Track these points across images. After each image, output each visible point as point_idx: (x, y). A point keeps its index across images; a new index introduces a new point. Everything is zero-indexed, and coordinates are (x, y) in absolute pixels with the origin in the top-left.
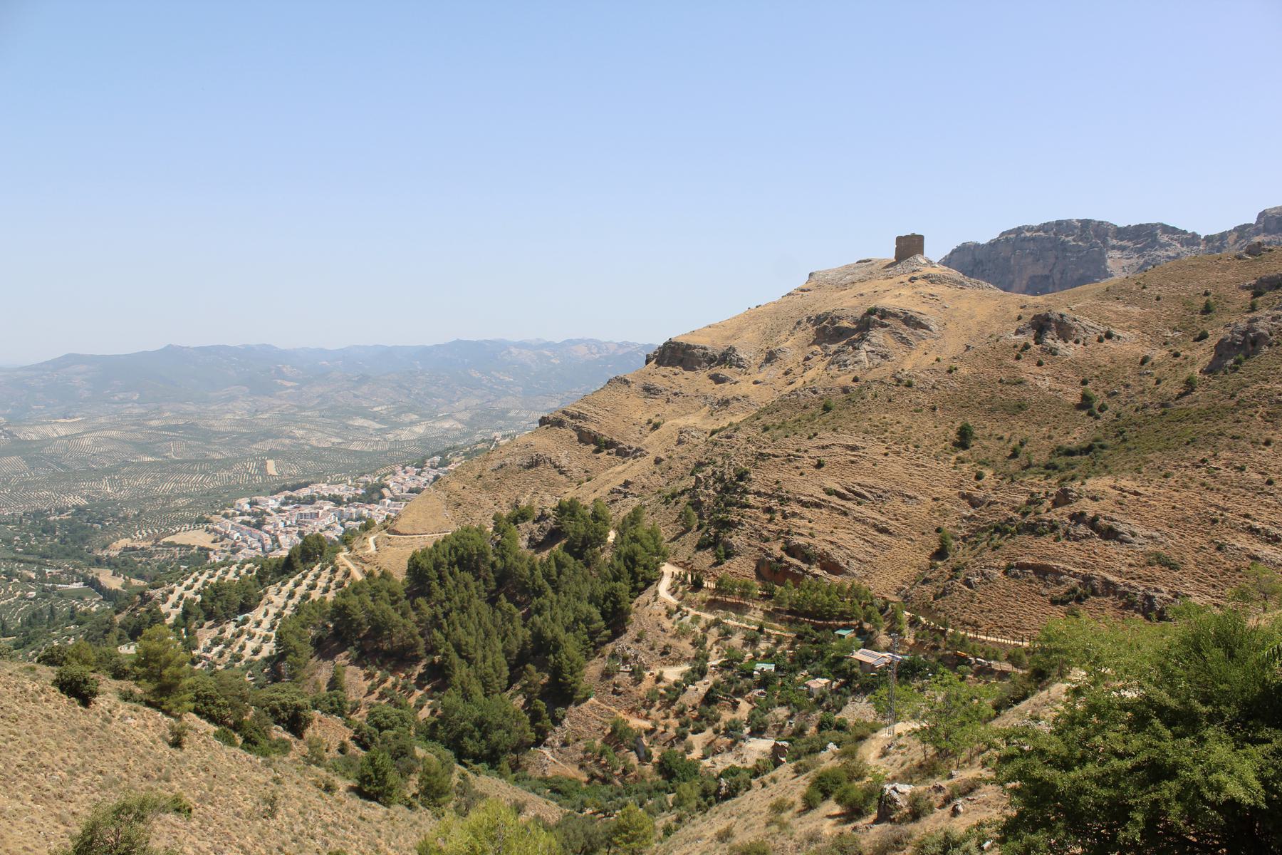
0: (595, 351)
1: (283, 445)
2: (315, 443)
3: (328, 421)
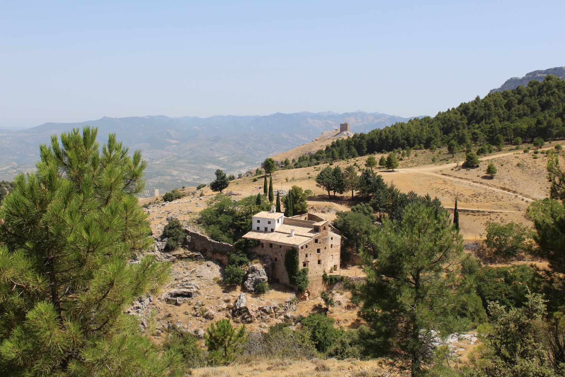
0: (360, 121)
1: (166, 180)
2: (184, 179)
3: (193, 166)
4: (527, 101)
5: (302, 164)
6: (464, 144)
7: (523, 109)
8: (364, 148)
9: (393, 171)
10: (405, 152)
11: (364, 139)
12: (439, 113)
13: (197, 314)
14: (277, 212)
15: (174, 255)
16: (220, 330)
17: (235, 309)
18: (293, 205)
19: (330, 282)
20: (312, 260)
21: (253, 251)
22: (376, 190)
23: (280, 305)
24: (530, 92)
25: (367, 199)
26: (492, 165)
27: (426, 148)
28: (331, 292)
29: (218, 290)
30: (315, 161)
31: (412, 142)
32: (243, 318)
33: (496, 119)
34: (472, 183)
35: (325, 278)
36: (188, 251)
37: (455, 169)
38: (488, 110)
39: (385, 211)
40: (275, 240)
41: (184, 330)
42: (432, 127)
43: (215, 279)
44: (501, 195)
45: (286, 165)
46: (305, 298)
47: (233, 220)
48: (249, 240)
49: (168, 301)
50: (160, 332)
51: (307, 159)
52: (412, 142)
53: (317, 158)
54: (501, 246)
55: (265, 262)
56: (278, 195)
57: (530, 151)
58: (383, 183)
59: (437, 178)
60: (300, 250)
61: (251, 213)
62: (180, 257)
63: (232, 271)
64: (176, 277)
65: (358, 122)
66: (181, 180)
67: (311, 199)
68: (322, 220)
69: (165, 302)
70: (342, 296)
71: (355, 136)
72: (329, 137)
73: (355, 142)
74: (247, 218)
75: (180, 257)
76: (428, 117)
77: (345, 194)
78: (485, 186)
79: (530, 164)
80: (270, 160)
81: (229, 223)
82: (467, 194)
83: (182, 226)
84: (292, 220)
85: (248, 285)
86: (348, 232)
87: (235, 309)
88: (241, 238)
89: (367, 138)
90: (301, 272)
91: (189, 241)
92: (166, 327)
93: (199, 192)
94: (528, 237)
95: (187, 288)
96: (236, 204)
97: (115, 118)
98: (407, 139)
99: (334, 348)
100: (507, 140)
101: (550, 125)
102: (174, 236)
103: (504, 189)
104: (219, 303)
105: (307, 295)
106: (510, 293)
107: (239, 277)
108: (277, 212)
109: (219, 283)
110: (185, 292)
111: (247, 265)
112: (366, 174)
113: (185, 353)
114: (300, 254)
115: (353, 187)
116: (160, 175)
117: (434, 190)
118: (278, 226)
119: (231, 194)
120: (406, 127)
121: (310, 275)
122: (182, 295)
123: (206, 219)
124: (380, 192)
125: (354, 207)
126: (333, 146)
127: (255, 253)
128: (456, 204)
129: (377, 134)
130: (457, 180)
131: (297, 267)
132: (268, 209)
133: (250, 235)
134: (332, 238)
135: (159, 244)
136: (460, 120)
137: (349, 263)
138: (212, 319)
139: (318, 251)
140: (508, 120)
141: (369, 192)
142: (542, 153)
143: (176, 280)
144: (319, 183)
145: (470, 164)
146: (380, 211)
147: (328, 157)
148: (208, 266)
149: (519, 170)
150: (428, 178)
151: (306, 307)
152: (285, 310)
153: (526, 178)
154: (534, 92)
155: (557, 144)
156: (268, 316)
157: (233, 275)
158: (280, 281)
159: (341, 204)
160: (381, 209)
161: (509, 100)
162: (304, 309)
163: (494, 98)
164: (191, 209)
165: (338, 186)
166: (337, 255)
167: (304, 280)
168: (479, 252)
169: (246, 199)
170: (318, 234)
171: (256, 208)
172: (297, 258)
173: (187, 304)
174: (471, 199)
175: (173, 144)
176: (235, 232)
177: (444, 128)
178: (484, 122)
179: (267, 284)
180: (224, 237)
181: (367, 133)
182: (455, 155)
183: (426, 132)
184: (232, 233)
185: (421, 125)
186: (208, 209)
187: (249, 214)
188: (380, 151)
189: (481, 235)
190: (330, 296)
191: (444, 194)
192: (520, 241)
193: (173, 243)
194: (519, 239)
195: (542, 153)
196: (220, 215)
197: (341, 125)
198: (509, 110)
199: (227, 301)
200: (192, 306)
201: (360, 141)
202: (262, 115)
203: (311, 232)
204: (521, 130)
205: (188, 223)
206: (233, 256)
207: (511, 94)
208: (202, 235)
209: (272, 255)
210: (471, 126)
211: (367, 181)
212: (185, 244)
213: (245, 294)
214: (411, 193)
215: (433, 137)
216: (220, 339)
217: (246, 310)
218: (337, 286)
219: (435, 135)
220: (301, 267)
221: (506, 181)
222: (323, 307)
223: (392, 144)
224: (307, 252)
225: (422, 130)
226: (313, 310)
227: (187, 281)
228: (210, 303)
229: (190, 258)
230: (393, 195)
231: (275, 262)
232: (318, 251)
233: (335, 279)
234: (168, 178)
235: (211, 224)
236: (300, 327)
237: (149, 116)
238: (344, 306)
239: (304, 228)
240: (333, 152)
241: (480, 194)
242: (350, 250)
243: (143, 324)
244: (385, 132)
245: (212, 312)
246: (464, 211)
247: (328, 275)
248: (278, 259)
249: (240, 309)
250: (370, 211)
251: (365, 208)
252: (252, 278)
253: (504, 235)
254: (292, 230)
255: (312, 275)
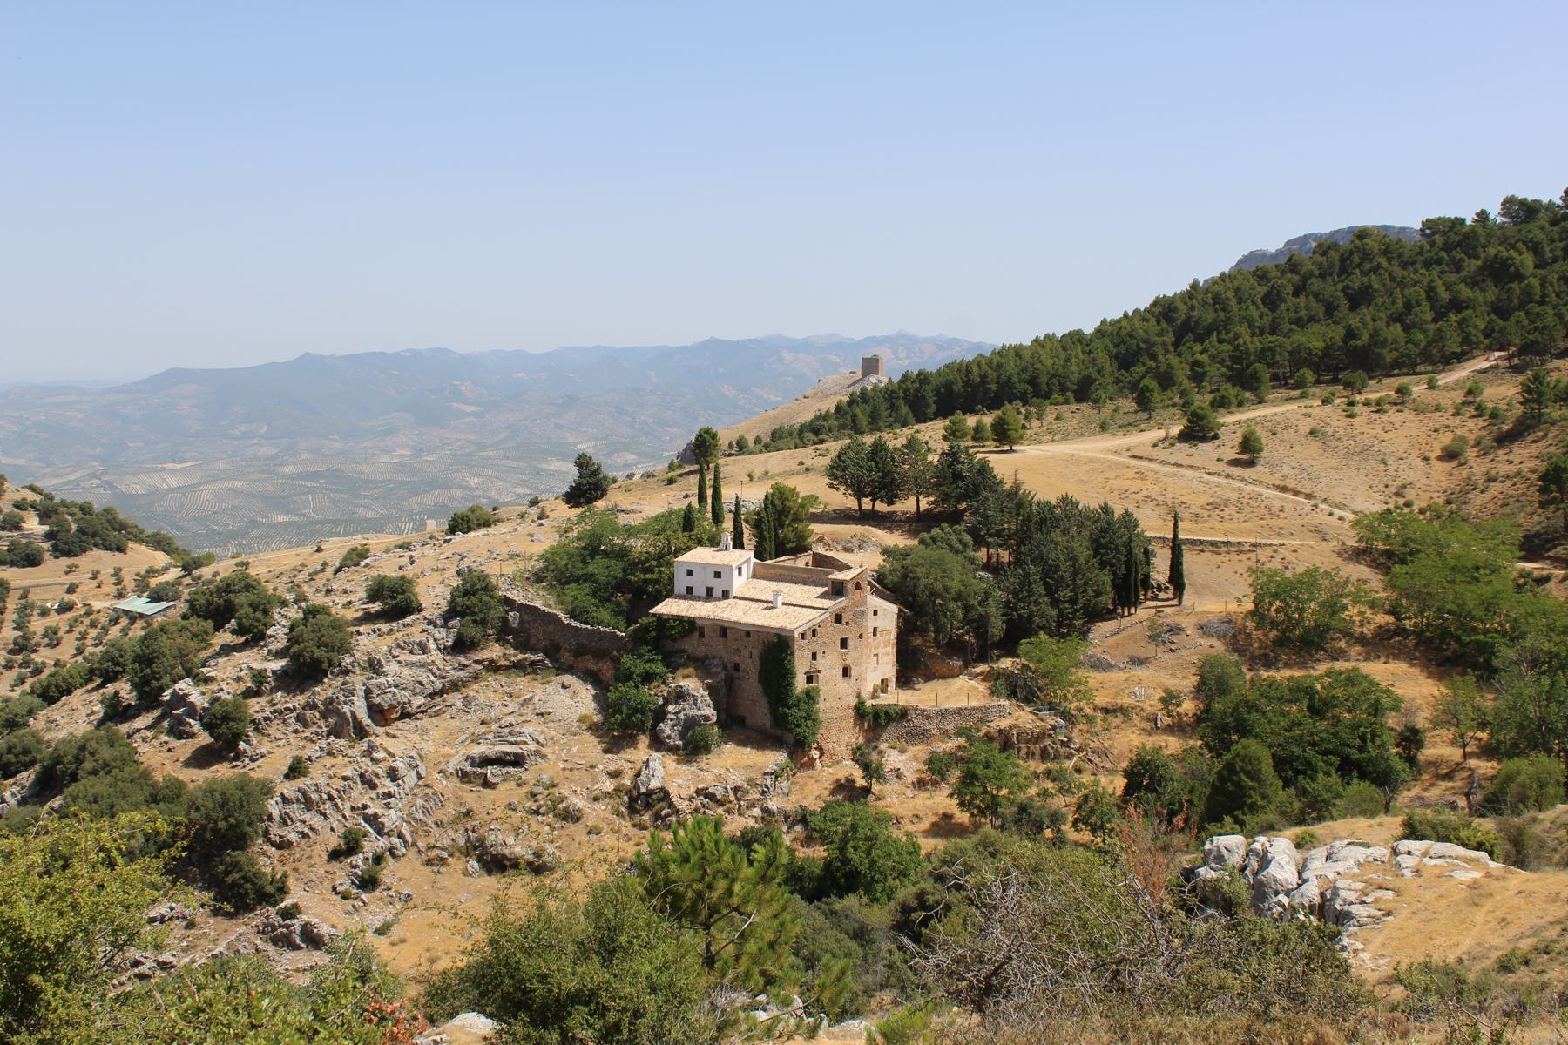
0: (903, 355)
1: (453, 498)
2: (494, 495)
3: (515, 464)
4: (1314, 289)
5: (780, 444)
7: (1307, 307)
8: (928, 406)
9: (1012, 451)
12: (1104, 322)
13: (539, 807)
15: (477, 662)
16: (686, 859)
17: (635, 793)
20: (829, 666)
21: (677, 646)
22: (977, 493)
23: (750, 782)
24: (1320, 266)
25: (955, 518)
26: (1253, 433)
27: (1079, 400)
29: (592, 746)
30: (810, 436)
31: (1044, 387)
32: (657, 816)
33: (1243, 329)
34: (1207, 477)
35: (860, 711)
36: (513, 651)
38: (1224, 310)
39: (1000, 546)
40: (734, 619)
41: (506, 851)
42: (1090, 352)
43: (582, 720)
44: (1277, 504)
45: (741, 447)
46: (811, 764)
48: (667, 620)
49: (464, 776)
50: (445, 855)
52: (1044, 387)
53: (816, 431)
54: (1290, 624)
55: (709, 675)
56: (737, 513)
57: (1337, 401)
59: (1119, 466)
60: (799, 642)
61: (669, 553)
62: (493, 667)
63: (624, 698)
64: (484, 716)
69: (456, 780)
70: (903, 757)
71: (905, 378)
74: (659, 566)
75: (493, 667)
76: (1079, 332)
77: (898, 507)
78: (1237, 484)
79: (1341, 431)
80: (708, 431)
82: (1197, 502)
83: (496, 588)
84: (773, 567)
85: (668, 731)
86: (914, 596)
87: (635, 793)
88: (647, 615)
89: (935, 382)
90: (802, 696)
91: (515, 625)
92: (462, 842)
93: (535, 511)
94: (1355, 603)
96: (630, 531)
97: (332, 356)
98: (1033, 382)
99: (912, 890)
100: (1275, 378)
101: (1377, 340)
103: (1284, 489)
104: (595, 780)
105: (815, 754)
106: (1323, 740)
109: (594, 728)
110: (507, 753)
111: (664, 682)
112: (952, 456)
113: (612, 1017)
114: (797, 653)
115: (920, 488)
118: (739, 584)
119: (616, 510)
120: (1027, 355)
121: (823, 706)
122: (500, 761)
123: (556, 569)
124: (987, 498)
125: (925, 535)
126: (851, 403)
127: (684, 651)
128: (1176, 526)
130: (1168, 469)
131: (791, 684)
132: (714, 542)
133: (669, 607)
134: (875, 613)
135: (440, 633)
136: (1158, 334)
137: (918, 675)
138: (578, 819)
139: (844, 643)
140: (1273, 333)
141: (959, 500)
142: (1367, 404)
143: (483, 722)
144: (836, 478)
145: (1198, 431)
146: (988, 546)
147: (842, 427)
148: (564, 687)
149: (1313, 446)
151: (816, 786)
153: (1333, 463)
154: (1331, 266)
155: (1396, 385)
156: (720, 810)
157: (630, 708)
158: (749, 721)
159: (890, 529)
161: (1273, 287)
162: (811, 790)
163: (1236, 283)
164: (517, 547)
165: (882, 486)
167: (808, 717)
168: (1237, 642)
169: (656, 519)
170: (842, 602)
171: (681, 538)
172: (791, 663)
174: (1206, 513)
175: (468, 415)
176: (630, 602)
178: (1214, 337)
179: (716, 729)
185: (1064, 348)
186: (561, 546)
187: (665, 557)
188: (969, 410)
189: (1239, 600)
190: (874, 757)
192: (1333, 613)
193: (473, 632)
194: (1334, 608)
195: (1367, 404)
198: (1272, 310)
200: (525, 789)
201: (918, 390)
203: (823, 596)
204: (1310, 354)
205: (512, 581)
206: (628, 661)
207: (1274, 273)
209: (725, 656)
210: (1183, 348)
213: (659, 755)
214: (1065, 500)
215: (1095, 375)
216: (690, 894)
217: (664, 795)
219: (1099, 372)
220: (800, 684)
221: (1286, 470)
223: (996, 393)
225: (1067, 360)
226: (832, 793)
227: (511, 725)
228: (572, 781)
229: (519, 666)
230: (1020, 505)
231: (735, 674)
232: (844, 643)
233: (887, 713)
234: (458, 493)
236: (802, 836)
237: (409, 351)
240: (854, 416)
241: (1226, 503)
242: (919, 641)
243: (400, 836)
244: (979, 365)
245: (578, 802)
246: (1193, 542)
247: (869, 703)
248: (742, 667)
249: (650, 793)
250: (965, 545)
251: (954, 538)
253: (1296, 598)
254: (776, 593)
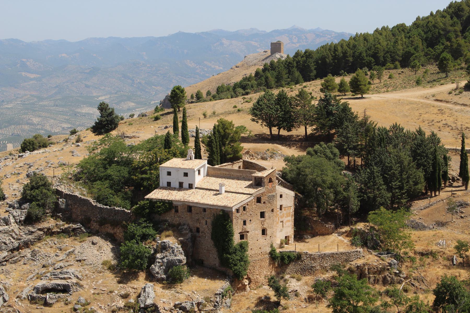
0: (295, 41)
2: (48, 128)
3: (61, 109)
6: (462, 58)
8: (311, 71)
9: (362, 98)
10: (375, 72)
11: (311, 58)
12: (418, 19)
14: (196, 158)
15: (40, 230)
18: (220, 148)
19: (282, 261)
20: (254, 228)
21: (162, 218)
22: (342, 123)
23: (207, 299)
25: (328, 138)
27: (403, 66)
28: (283, 277)
29: (110, 280)
30: (240, 90)
31: (382, 59)
35: (273, 256)
36: (62, 223)
37: (454, 93)
39: (356, 155)
40: (196, 201)
42: (409, 37)
43: (104, 263)
45: (198, 98)
47: (129, 173)
48: (156, 202)
49: (32, 300)
51: (228, 90)
52: (382, 59)
53: (244, 88)
55: (181, 235)
58: (352, 114)
59: (428, 106)
60: (235, 215)
62: (49, 232)
63: (130, 250)
64: (44, 263)
65: (293, 43)
66: (45, 130)
67: (245, 140)
68: (264, 169)
69: (27, 302)
70: (299, 283)
72: (255, 62)
73: (297, 63)
74: (150, 170)
75: (49, 232)
77: (294, 132)
80: (178, 88)
81: (124, 177)
83: (51, 184)
84: (219, 169)
86: (304, 186)
88: (144, 199)
89: (315, 56)
90: (238, 247)
91: (63, 207)
95: (61, 279)
96: (132, 149)
98: (375, 56)
102: (39, 200)
104: (113, 300)
105: (246, 282)
107: (141, 259)
108: (196, 158)
109: (112, 269)
110: (59, 285)
111: (154, 240)
112: (326, 101)
114: (234, 221)
115: (307, 121)
116: (14, 124)
117: (427, 122)
118: (199, 180)
119: (124, 136)
120: (371, 40)
124: (347, 127)
125: (310, 149)
126: (265, 70)
127: (166, 221)
129: (330, 50)
130: (458, 107)
131: (231, 240)
132: (183, 155)
133: (157, 195)
134: (281, 196)
135: (17, 213)
139: (262, 215)
141: (331, 128)
143: (44, 266)
144: (256, 115)
146: (349, 155)
147: (259, 85)
148: (93, 244)
150: (415, 106)
151: (247, 301)
152: (215, 306)
158: (205, 263)
159: (289, 146)
160: (350, 151)
165: (284, 120)
166: (289, 221)
167: (241, 260)
169: (148, 141)
170: (261, 190)
171: (164, 153)
172: (231, 227)
173: (63, 303)
175: (31, 80)
176: (133, 191)
177: (427, 38)
179: (186, 268)
180: (118, 200)
181: (315, 50)
182: (449, 74)
183: (402, 45)
184: (129, 192)
185: (394, 35)
187: (153, 164)
188: (336, 73)
190: (282, 283)
191: (442, 128)
193: (37, 211)
196: (110, 166)
197: (272, 44)
199: (125, 296)
200: (70, 306)
201: (305, 62)
202: (157, 35)
203: (249, 186)
205: (61, 181)
206: (132, 227)
208: (83, 197)
209: (191, 223)
211: (327, 112)
212: (56, 211)
213: (151, 284)
218: (291, 267)
219: (415, 49)
220: (236, 240)
222: (272, 300)
223: (353, 63)
224: (245, 217)
225: (396, 42)
226: (257, 305)
227: (61, 267)
228: (99, 301)
229: (65, 232)
230: (368, 130)
231: (197, 234)
232: (262, 215)
233: (289, 257)
235: (95, 181)
238: (303, 298)
239: (239, 182)
240: (267, 78)
242: (308, 213)
244: (342, 46)
247: (278, 251)
248: (201, 230)
250: (335, 155)
251: (328, 151)
252: (161, 259)
254: (221, 185)
255: (253, 252)
